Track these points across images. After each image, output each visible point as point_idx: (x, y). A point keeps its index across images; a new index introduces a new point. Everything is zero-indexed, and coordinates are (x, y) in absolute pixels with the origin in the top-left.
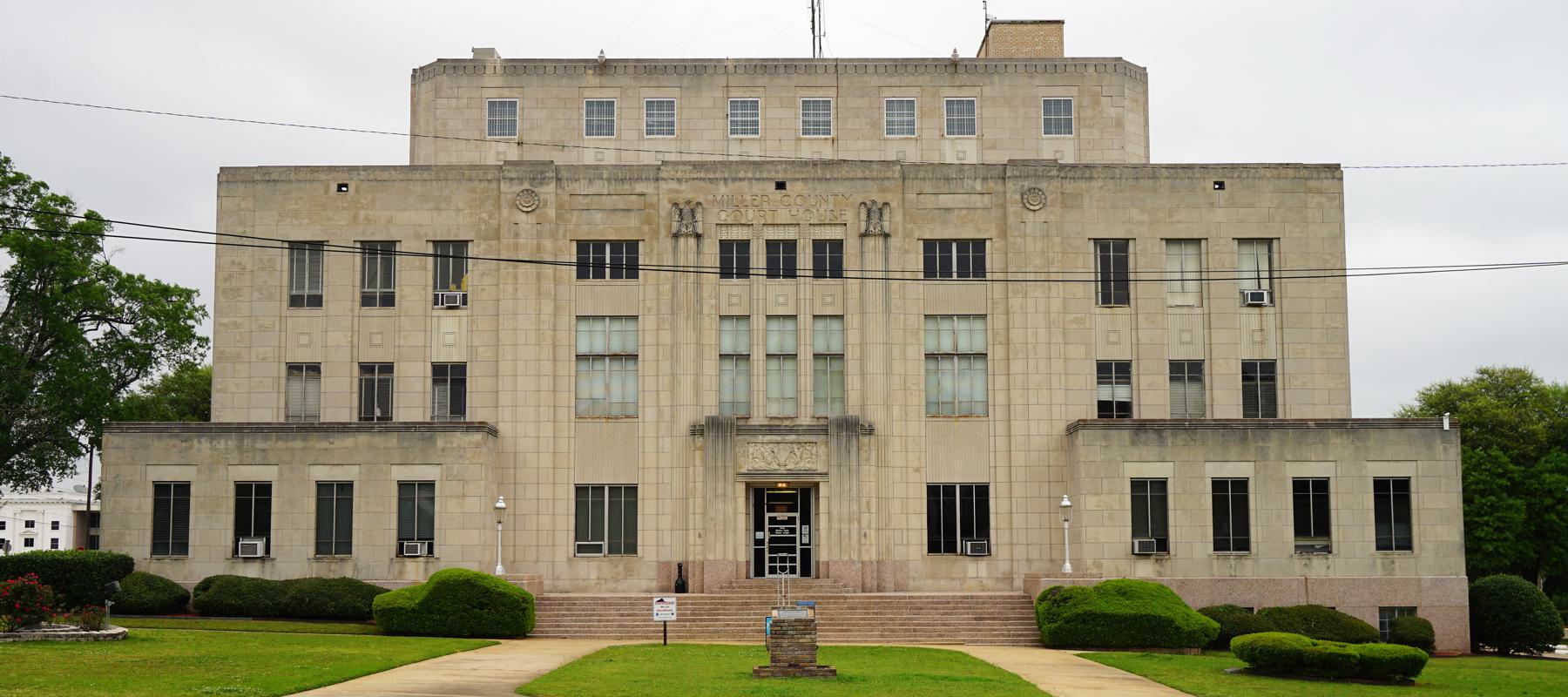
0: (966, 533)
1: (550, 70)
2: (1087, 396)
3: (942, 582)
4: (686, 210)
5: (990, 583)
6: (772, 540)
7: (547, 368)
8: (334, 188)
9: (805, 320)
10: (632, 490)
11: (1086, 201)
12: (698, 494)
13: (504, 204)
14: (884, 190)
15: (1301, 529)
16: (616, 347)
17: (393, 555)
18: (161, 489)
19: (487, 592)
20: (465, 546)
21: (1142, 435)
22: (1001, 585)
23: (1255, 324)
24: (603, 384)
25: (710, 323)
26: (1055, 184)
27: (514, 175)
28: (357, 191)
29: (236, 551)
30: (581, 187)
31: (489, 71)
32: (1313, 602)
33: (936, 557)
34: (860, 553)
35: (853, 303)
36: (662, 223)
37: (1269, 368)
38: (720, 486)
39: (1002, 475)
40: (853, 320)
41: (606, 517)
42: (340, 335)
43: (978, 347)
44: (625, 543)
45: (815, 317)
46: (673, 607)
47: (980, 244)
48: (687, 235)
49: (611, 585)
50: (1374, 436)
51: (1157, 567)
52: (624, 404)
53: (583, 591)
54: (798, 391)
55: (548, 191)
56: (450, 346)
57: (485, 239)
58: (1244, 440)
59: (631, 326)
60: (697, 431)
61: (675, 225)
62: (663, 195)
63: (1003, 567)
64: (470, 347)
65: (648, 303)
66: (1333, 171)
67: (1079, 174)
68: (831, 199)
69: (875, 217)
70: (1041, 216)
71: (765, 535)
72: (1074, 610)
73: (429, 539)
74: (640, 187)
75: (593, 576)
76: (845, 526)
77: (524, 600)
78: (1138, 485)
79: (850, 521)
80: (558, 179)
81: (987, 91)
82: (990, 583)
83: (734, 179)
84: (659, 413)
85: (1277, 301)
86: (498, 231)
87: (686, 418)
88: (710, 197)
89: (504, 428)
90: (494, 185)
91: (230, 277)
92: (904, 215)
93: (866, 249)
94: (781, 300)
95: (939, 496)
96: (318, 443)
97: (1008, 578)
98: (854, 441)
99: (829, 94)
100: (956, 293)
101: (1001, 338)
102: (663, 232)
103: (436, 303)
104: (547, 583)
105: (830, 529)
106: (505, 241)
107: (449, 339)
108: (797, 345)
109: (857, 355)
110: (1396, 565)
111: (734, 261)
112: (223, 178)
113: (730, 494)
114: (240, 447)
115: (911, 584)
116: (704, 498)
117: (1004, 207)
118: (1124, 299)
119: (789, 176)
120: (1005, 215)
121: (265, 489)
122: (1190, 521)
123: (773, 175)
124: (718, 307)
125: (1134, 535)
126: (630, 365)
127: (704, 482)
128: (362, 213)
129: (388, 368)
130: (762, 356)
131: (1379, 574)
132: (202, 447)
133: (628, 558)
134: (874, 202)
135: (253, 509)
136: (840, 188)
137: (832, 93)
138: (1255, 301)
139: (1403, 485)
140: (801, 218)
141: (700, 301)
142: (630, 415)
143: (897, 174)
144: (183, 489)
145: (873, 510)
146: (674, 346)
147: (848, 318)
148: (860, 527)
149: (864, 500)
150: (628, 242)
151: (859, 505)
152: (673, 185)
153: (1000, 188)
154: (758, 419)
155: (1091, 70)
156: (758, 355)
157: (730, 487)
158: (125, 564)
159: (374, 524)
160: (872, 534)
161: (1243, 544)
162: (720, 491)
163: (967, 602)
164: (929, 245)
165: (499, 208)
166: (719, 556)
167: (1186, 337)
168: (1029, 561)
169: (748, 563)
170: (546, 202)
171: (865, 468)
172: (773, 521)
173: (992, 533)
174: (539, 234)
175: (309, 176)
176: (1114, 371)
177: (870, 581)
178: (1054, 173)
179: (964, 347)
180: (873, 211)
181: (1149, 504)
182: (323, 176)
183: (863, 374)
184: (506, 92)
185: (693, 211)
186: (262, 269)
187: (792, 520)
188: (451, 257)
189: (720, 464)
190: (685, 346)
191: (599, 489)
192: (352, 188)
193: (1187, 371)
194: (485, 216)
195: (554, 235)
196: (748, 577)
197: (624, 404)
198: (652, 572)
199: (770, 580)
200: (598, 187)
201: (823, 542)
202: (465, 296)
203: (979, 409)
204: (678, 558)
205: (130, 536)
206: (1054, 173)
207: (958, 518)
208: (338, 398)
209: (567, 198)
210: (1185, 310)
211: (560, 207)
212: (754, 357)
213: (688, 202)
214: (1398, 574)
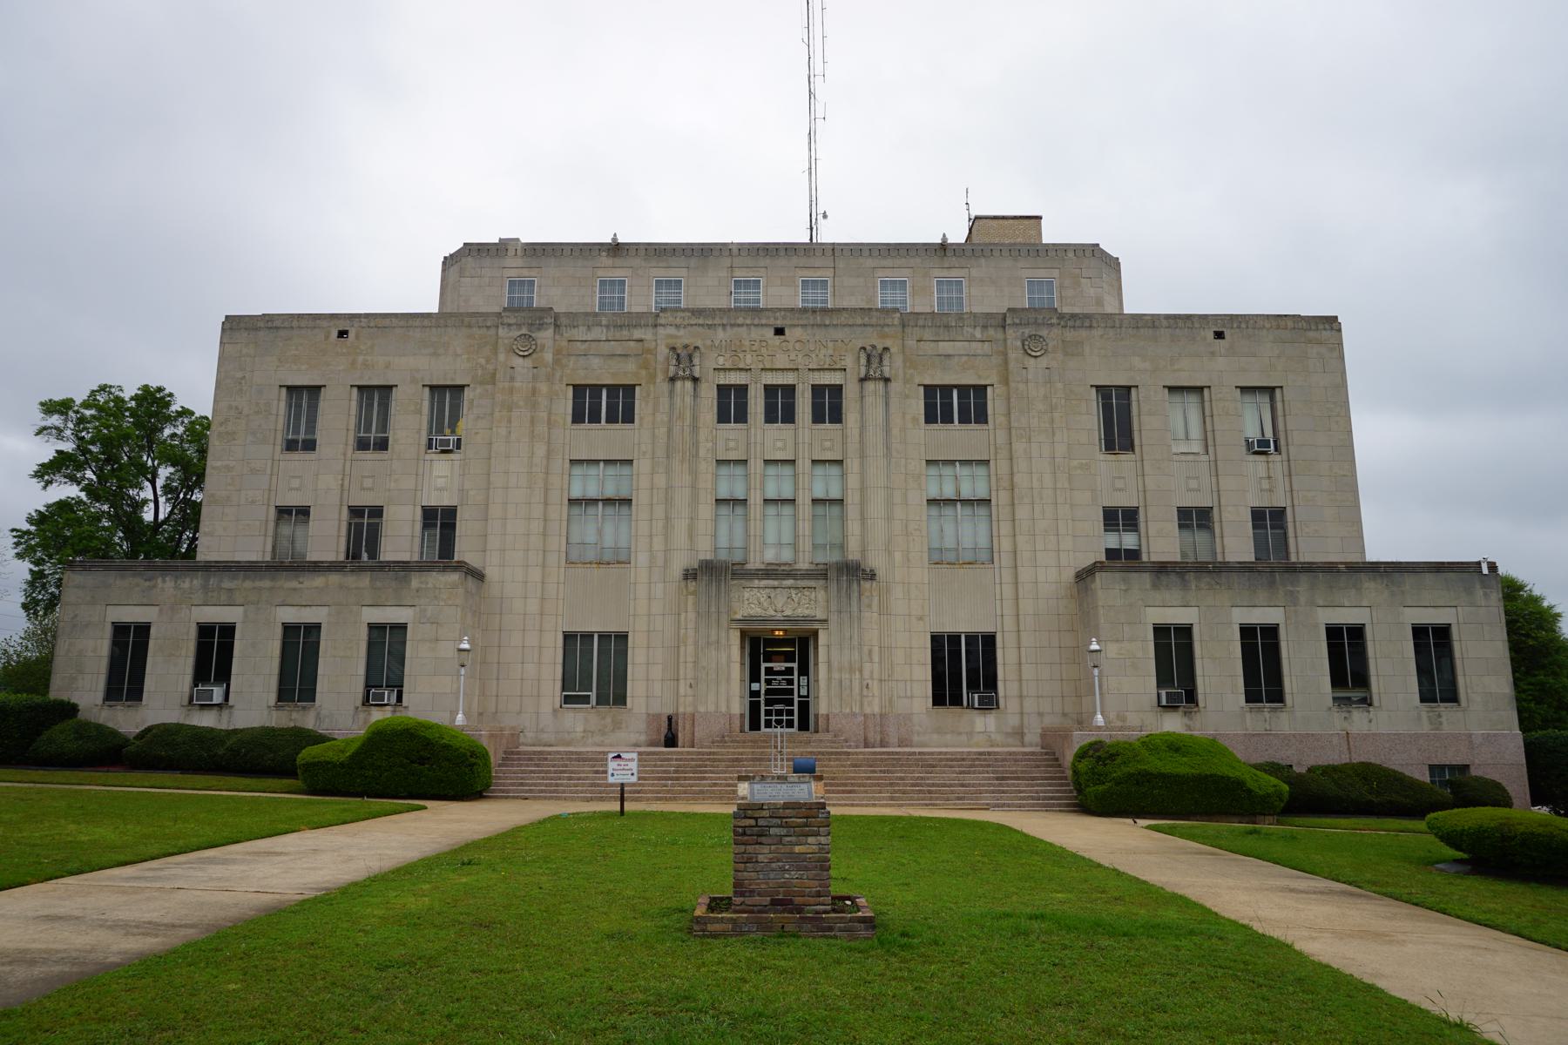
0: (973, 686)
1: (567, 252)
2: (1097, 542)
3: (949, 737)
4: (683, 353)
5: (998, 738)
6: (768, 692)
7: (537, 511)
8: (335, 334)
9: (804, 464)
10: (622, 638)
11: (1087, 349)
12: (690, 641)
13: (501, 349)
14: (883, 336)
15: (1338, 680)
16: (610, 492)
17: (359, 703)
18: (120, 630)
19: (428, 744)
20: (436, 697)
21: (1163, 578)
22: (1010, 740)
23: (1262, 472)
24: (597, 529)
25: (706, 468)
26: (1056, 331)
27: (512, 321)
28: (357, 337)
29: (191, 700)
30: (580, 333)
31: (511, 252)
32: (1356, 759)
33: (941, 710)
34: (862, 705)
35: (853, 446)
36: (659, 367)
37: (1278, 515)
38: (713, 632)
39: (1009, 623)
40: (853, 465)
41: (595, 667)
42: (328, 481)
43: (982, 493)
44: (615, 694)
45: (814, 462)
46: (634, 766)
47: (981, 390)
48: (684, 379)
49: (597, 739)
50: (1409, 580)
51: (1186, 720)
52: (616, 549)
53: (568, 744)
54: (796, 536)
55: (546, 336)
56: (440, 489)
57: (481, 383)
58: (1272, 584)
59: (626, 470)
60: (689, 575)
61: (672, 369)
62: (660, 341)
63: (1013, 721)
64: (461, 490)
65: (643, 448)
66: (1331, 322)
67: (1078, 323)
68: (830, 345)
69: (875, 361)
70: (1043, 362)
71: (761, 686)
72: (1126, 770)
73: (397, 686)
74: (638, 333)
75: (580, 728)
76: (846, 676)
77: (473, 754)
78: (1161, 631)
79: (851, 670)
80: (557, 326)
81: (974, 272)
82: (998, 738)
83: (732, 325)
84: (652, 558)
85: (1283, 449)
86: (493, 375)
87: (681, 562)
88: (709, 343)
89: (491, 573)
90: (492, 331)
91: (227, 420)
92: (904, 361)
93: (866, 393)
94: (779, 444)
95: (944, 649)
96: (288, 583)
97: (1019, 733)
98: (855, 586)
99: (827, 275)
100: (957, 437)
101: (1005, 483)
102: (660, 377)
103: (430, 447)
104: (529, 736)
105: (829, 679)
106: (500, 385)
107: (441, 482)
108: (796, 490)
109: (857, 498)
110: (1443, 720)
111: (731, 405)
112: (228, 326)
113: (723, 641)
114: (205, 588)
115: (916, 738)
116: (696, 643)
117: (1005, 354)
118: (1129, 446)
119: (788, 322)
120: (1006, 362)
121: (228, 631)
122: (1219, 670)
123: (772, 321)
124: (714, 450)
125: (1159, 685)
126: (624, 510)
127: (697, 630)
128: (360, 359)
129: (377, 512)
130: (759, 501)
131: (1426, 728)
132: (167, 586)
133: (615, 710)
134: (874, 347)
135: (214, 653)
136: (839, 334)
137: (830, 273)
138: (1260, 448)
139: (1443, 632)
140: (800, 362)
141: (696, 444)
142: (620, 560)
143: (896, 322)
144: (143, 630)
145: (876, 658)
146: (669, 488)
147: (848, 463)
148: (862, 679)
149: (866, 649)
150: (624, 386)
151: (860, 653)
152: (671, 331)
153: (1000, 335)
154: (755, 563)
155: (1071, 254)
156: (756, 499)
157: (723, 634)
158: (69, 710)
159: (341, 670)
160: (875, 686)
161: (1277, 696)
162: (713, 638)
163: (982, 760)
164: (929, 390)
165: (496, 353)
166: (712, 708)
167: (1193, 484)
168: (1040, 714)
169: (742, 716)
170: (543, 346)
171: (866, 614)
172: (769, 671)
173: (1000, 685)
174: (535, 378)
175: (311, 324)
176: (1120, 518)
177: (874, 736)
178: (1054, 321)
179: (966, 493)
180: (874, 357)
181: (1174, 654)
182: (324, 324)
183: (863, 519)
184: (525, 272)
185: (690, 357)
186: (257, 413)
187: (789, 671)
189: (713, 609)
190: (685, 492)
191: (588, 637)
192: (352, 335)
193: (1195, 519)
194: (483, 361)
195: (550, 379)
196: (742, 731)
197: (616, 549)
198: (641, 725)
199: (765, 734)
200: (598, 333)
201: (822, 693)
202: (459, 440)
203: (984, 556)
204: (670, 712)
205: (82, 683)
206: (1054, 321)
207: (963, 670)
208: (326, 538)
209: (564, 343)
210: (1190, 458)
211: (558, 352)
212: (751, 501)
213: (686, 347)
214: (1447, 728)
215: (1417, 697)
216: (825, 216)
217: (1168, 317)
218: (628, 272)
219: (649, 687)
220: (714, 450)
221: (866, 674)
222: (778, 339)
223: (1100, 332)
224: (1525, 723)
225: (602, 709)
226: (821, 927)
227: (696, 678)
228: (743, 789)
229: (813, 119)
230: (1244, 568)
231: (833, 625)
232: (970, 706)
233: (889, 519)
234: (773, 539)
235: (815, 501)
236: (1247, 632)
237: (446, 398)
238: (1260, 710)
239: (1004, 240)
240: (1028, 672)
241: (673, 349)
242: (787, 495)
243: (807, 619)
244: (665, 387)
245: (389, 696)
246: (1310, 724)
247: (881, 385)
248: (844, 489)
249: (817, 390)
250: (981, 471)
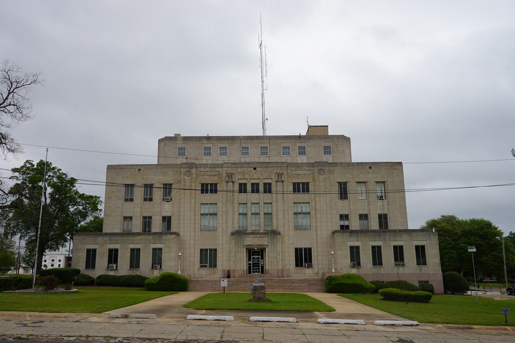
0: (306, 261)
1: (194, 139)
2: (337, 224)
4: (230, 175)
5: (312, 275)
7: (193, 217)
8: (137, 170)
9: (262, 204)
10: (215, 250)
14: (282, 170)
15: (396, 260)
16: (211, 212)
18: (88, 251)
19: (176, 278)
20: (170, 265)
23: (381, 204)
24: (207, 222)
26: (327, 168)
28: (143, 171)
29: (108, 268)
30: (202, 169)
31: (179, 139)
33: (298, 268)
37: (385, 216)
39: (315, 245)
40: (274, 204)
41: (208, 258)
42: (137, 209)
43: (308, 211)
44: (213, 265)
46: (226, 283)
47: (308, 184)
49: (209, 276)
52: (213, 227)
55: (193, 170)
57: (177, 183)
59: (215, 206)
60: (233, 234)
62: (224, 171)
64: (172, 212)
66: (400, 164)
70: (324, 176)
73: (160, 264)
74: (218, 169)
75: (205, 274)
76: (273, 259)
78: (352, 248)
79: (274, 258)
81: (309, 144)
82: (312, 275)
86: (180, 181)
89: (181, 234)
90: (179, 169)
95: (298, 251)
96: (131, 238)
97: (317, 274)
99: (267, 145)
100: (301, 197)
102: (224, 181)
105: (269, 260)
107: (167, 210)
109: (276, 213)
111: (242, 188)
114: (110, 239)
116: (235, 252)
118: (346, 198)
120: (314, 176)
121: (116, 251)
122: (366, 257)
124: (238, 201)
125: (351, 262)
126: (215, 217)
128: (144, 177)
129: (150, 218)
130: (250, 214)
131: (418, 272)
132: (100, 239)
133: (214, 269)
135: (113, 256)
136: (271, 169)
137: (268, 144)
139: (423, 247)
140: (260, 177)
141: (234, 199)
142: (215, 230)
144: (94, 251)
147: (273, 204)
150: (214, 184)
152: (227, 169)
153: (313, 169)
155: (336, 138)
156: (249, 214)
157: (242, 249)
158: (78, 271)
161: (381, 264)
162: (239, 250)
163: (306, 281)
164: (294, 184)
166: (239, 268)
168: (323, 269)
171: (278, 244)
172: (253, 258)
174: (191, 182)
176: (344, 217)
177: (280, 275)
179: (304, 211)
180: (280, 175)
181: (355, 252)
182: (134, 167)
183: (277, 218)
184: (183, 145)
185: (232, 176)
187: (258, 258)
188: (167, 188)
190: (229, 212)
191: (206, 250)
192: (142, 170)
193: (364, 217)
195: (195, 182)
197: (213, 227)
200: (207, 169)
201: (267, 264)
203: (308, 228)
205: (80, 265)
207: (303, 257)
208: (137, 226)
211: (197, 175)
212: (248, 214)
213: (231, 173)
214: (423, 272)
215: (416, 264)
216: (267, 120)
217: (357, 163)
218: (212, 145)
220: (238, 201)
221: (278, 259)
222: (255, 171)
223: (339, 167)
224: (443, 271)
225: (211, 269)
226: (264, 301)
227: (235, 261)
228: (254, 284)
229: (263, 90)
230: (374, 231)
231: (270, 246)
232: (305, 267)
233: (284, 218)
234: (253, 224)
235: (265, 214)
236: (373, 247)
237: (167, 188)
238: (376, 267)
239: (317, 134)
241: (227, 174)
242: (257, 212)
243: (263, 245)
244: (225, 184)
245: (158, 267)
247: (281, 183)
249: (265, 184)
250: (308, 205)
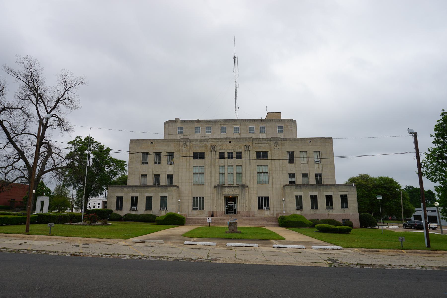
0: (265, 206)
2: (287, 180)
5: (269, 215)
7: (188, 175)
9: (235, 167)
10: (203, 198)
14: (249, 143)
15: (327, 205)
16: (200, 172)
18: (118, 197)
20: (172, 208)
23: (317, 167)
24: (198, 178)
26: (280, 141)
30: (194, 143)
33: (260, 210)
37: (320, 175)
39: (271, 195)
40: (244, 166)
41: (198, 203)
42: (150, 169)
44: (202, 208)
47: (267, 152)
50: (340, 187)
52: (202, 182)
58: (316, 188)
59: (203, 168)
60: (215, 187)
62: (209, 144)
63: (272, 212)
70: (278, 147)
74: (205, 143)
81: (267, 125)
82: (269, 215)
86: (179, 150)
87: (213, 184)
89: (180, 186)
95: (260, 199)
96: (146, 189)
97: (273, 214)
99: (239, 126)
100: (262, 161)
104: (188, 215)
107: (170, 170)
111: (222, 156)
114: (132, 190)
118: (293, 162)
122: (306, 203)
126: (203, 175)
129: (159, 175)
132: (125, 190)
135: (134, 201)
136: (241, 142)
139: (346, 196)
140: (234, 148)
142: (203, 184)
144: (122, 197)
146: (211, 171)
154: (226, 185)
156: (226, 173)
158: (111, 211)
159: (156, 204)
161: (317, 207)
163: (265, 219)
164: (257, 153)
167: (305, 169)
172: (229, 203)
174: (187, 151)
176: (292, 175)
179: (264, 171)
180: (247, 147)
181: (299, 199)
183: (245, 176)
187: (233, 203)
191: (197, 198)
193: (305, 175)
195: (189, 151)
197: (202, 182)
200: (197, 143)
201: (239, 208)
203: (267, 183)
205: (112, 207)
207: (263, 203)
208: (150, 181)
211: (190, 146)
214: (346, 213)
219: (208, 206)
226: (237, 232)
229: (236, 88)
232: (265, 209)
234: (229, 180)
235: (237, 173)
236: (312, 196)
237: (170, 155)
239: (274, 118)
240: (275, 203)
244: (210, 152)
246: (322, 212)
248: (242, 171)
